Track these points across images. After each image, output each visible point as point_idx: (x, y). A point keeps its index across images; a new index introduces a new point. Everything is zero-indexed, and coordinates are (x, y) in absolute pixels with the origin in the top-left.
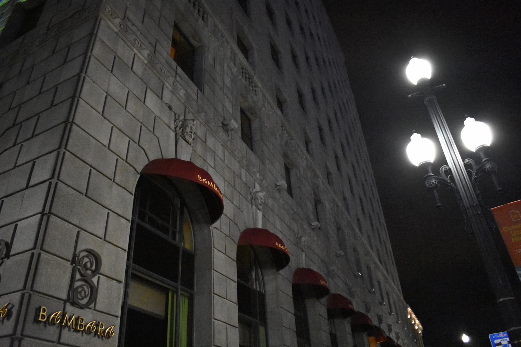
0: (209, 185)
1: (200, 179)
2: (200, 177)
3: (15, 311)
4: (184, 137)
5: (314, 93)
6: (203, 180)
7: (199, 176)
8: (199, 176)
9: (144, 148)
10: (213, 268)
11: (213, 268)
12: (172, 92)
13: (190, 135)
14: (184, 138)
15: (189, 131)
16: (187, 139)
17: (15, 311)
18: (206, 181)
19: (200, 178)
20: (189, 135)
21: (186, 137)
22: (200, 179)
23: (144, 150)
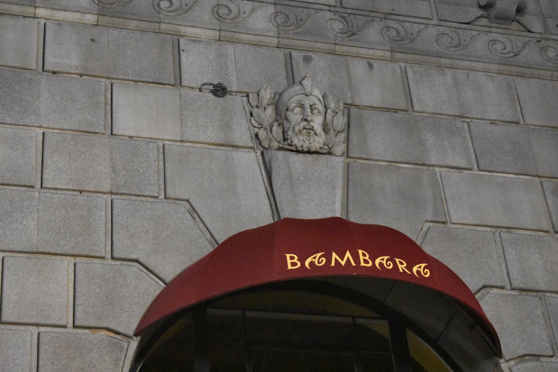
0: (401, 271)
1: (366, 262)
2: (364, 255)
3: (380, 19)
4: (291, 145)
5: (71, 25)
6: (377, 261)
7: (360, 252)
8: (360, 252)
9: (134, 257)
10: (451, 221)
11: (451, 221)
12: (186, 33)
13: (305, 131)
14: (293, 148)
15: (299, 117)
16: (302, 146)
17: (380, 19)
18: (387, 260)
19: (367, 258)
20: (300, 131)
21: (295, 141)
22: (366, 262)
23: (137, 261)
